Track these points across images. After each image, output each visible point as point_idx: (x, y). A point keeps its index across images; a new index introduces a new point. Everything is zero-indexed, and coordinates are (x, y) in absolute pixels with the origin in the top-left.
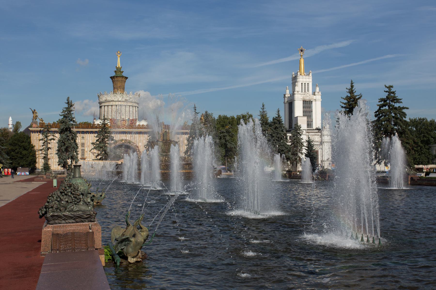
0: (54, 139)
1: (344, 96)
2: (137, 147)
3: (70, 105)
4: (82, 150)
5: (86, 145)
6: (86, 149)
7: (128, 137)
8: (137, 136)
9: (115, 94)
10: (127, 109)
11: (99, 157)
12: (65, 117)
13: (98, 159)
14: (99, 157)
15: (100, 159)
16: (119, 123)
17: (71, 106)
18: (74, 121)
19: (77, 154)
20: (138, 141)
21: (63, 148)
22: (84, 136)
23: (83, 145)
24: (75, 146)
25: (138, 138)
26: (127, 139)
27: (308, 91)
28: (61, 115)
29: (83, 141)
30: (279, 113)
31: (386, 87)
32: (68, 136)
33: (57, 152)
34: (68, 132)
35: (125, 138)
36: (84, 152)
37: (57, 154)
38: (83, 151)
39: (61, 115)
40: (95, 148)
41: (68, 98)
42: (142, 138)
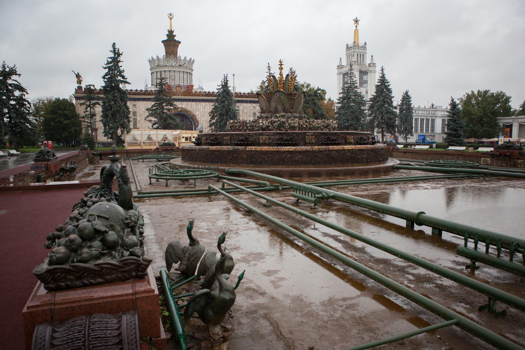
3: (117, 54)
4: (134, 119)
5: (138, 114)
6: (138, 119)
8: (194, 103)
9: (168, 59)
10: (181, 75)
11: (155, 126)
12: (109, 68)
13: (155, 129)
14: (155, 126)
15: (157, 128)
16: (174, 90)
17: (119, 55)
18: (123, 77)
20: (195, 110)
21: (110, 113)
23: (135, 113)
24: (126, 110)
25: (195, 107)
26: (184, 107)
28: (105, 68)
29: (135, 109)
30: (383, 72)
32: (115, 97)
33: (174, 34)
34: (116, 91)
35: (181, 106)
36: (136, 122)
37: (101, 121)
38: (135, 120)
39: (105, 68)
40: (151, 115)
41: (114, 44)
42: (199, 106)
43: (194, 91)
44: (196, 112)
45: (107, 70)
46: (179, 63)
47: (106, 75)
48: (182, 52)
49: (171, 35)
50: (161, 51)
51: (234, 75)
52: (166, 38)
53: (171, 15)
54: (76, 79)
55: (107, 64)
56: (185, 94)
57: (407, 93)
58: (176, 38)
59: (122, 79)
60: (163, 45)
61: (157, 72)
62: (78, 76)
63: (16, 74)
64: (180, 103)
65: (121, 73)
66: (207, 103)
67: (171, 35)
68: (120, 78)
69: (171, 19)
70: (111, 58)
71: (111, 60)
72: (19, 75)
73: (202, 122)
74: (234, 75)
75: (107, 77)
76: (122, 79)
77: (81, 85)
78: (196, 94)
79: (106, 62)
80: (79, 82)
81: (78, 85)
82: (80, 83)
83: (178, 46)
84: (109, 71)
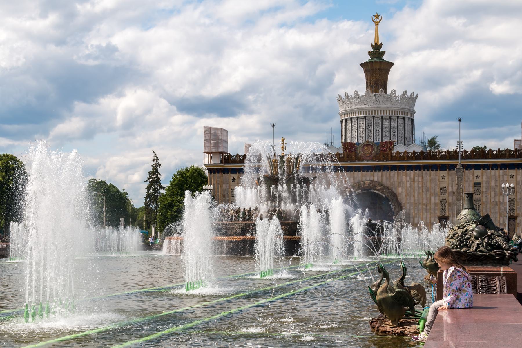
7: (377, 176)
8: (394, 173)
16: (360, 152)
25: (396, 179)
48: (396, 82)
49: (377, 51)
50: (357, 83)
52: (367, 58)
53: (377, 16)
56: (377, 158)
58: (385, 58)
66: (418, 172)
67: (377, 51)
69: (377, 24)
73: (408, 206)
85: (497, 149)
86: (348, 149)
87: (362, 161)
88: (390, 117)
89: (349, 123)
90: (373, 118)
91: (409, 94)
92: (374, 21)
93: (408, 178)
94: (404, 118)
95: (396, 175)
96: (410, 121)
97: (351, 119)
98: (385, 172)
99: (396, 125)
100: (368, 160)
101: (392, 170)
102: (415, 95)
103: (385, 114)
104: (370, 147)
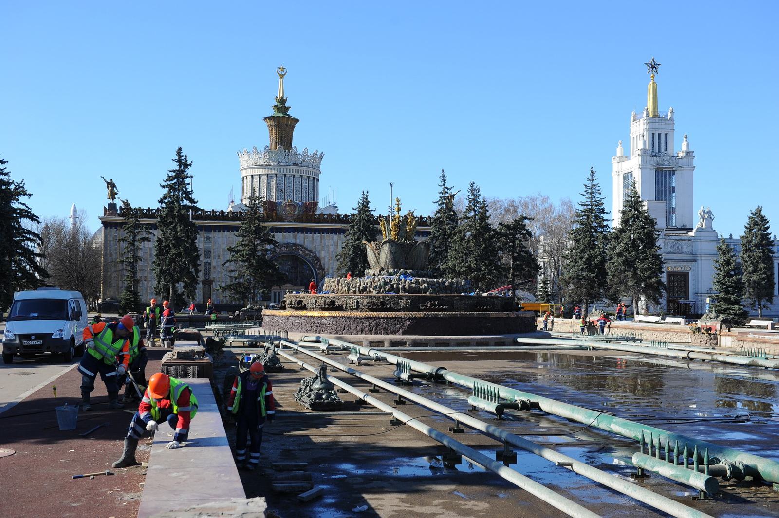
0: (148, 240)
1: (486, 194)
2: (318, 259)
3: (183, 163)
4: (206, 263)
6: (214, 263)
7: (299, 238)
8: (317, 236)
12: (171, 188)
17: (186, 166)
18: (192, 201)
19: (197, 271)
22: (210, 236)
23: (208, 253)
25: (318, 242)
27: (666, 149)
28: (164, 187)
31: (353, 209)
33: (287, 105)
35: (293, 242)
36: (210, 269)
39: (164, 187)
41: (180, 149)
43: (318, 212)
44: (320, 252)
45: (166, 190)
46: (294, 160)
47: (165, 198)
48: (301, 141)
49: (282, 106)
51: (391, 185)
54: (108, 191)
55: (167, 180)
56: (299, 220)
57: (759, 211)
59: (189, 204)
60: (265, 125)
61: (252, 176)
62: (111, 185)
63: (25, 194)
64: (292, 234)
65: (187, 194)
67: (282, 106)
68: (186, 202)
69: (282, 76)
70: (174, 171)
71: (174, 174)
72: (30, 195)
74: (391, 185)
75: (166, 201)
76: (189, 204)
77: (115, 201)
78: (323, 219)
79: (166, 178)
80: (113, 195)
81: (109, 201)
82: (113, 198)
83: (294, 127)
84: (170, 191)
85: (427, 217)
86: (269, 208)
87: (284, 222)
88: (302, 176)
89: (256, 179)
90: (285, 176)
91: (311, 152)
92: (279, 74)
93: (331, 242)
94: (308, 177)
95: (319, 239)
96: (311, 182)
97: (260, 175)
98: (309, 235)
99: (307, 185)
100: (289, 221)
101: (315, 233)
102: (319, 153)
103: (297, 173)
104: (292, 207)
